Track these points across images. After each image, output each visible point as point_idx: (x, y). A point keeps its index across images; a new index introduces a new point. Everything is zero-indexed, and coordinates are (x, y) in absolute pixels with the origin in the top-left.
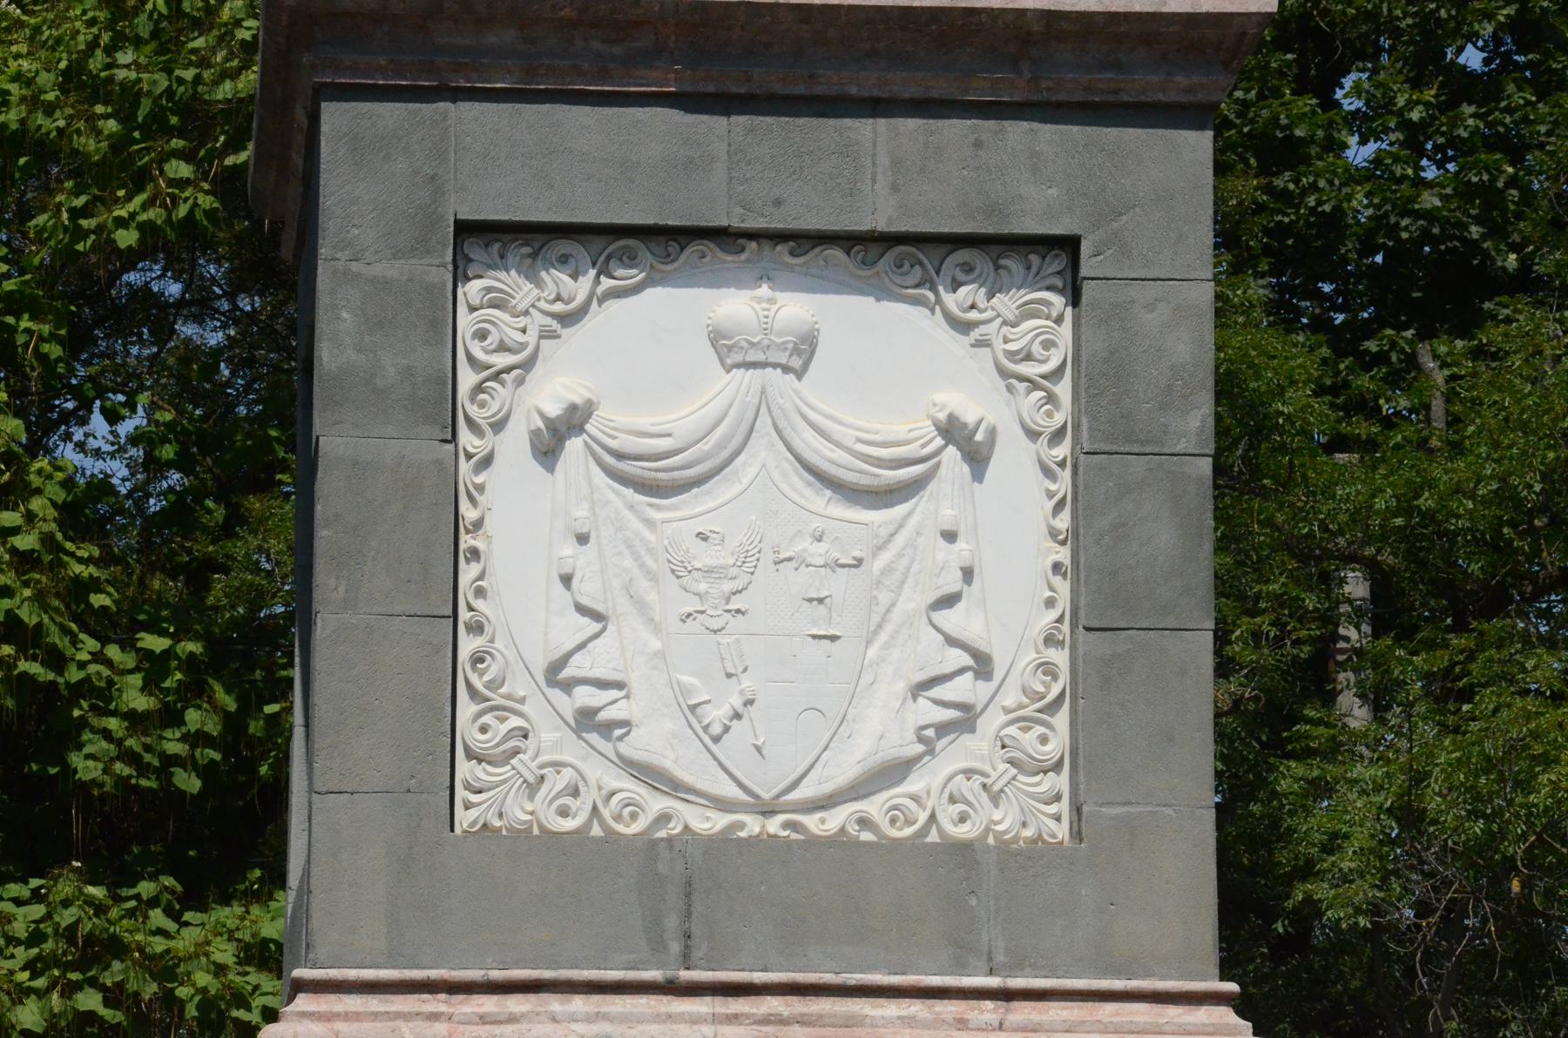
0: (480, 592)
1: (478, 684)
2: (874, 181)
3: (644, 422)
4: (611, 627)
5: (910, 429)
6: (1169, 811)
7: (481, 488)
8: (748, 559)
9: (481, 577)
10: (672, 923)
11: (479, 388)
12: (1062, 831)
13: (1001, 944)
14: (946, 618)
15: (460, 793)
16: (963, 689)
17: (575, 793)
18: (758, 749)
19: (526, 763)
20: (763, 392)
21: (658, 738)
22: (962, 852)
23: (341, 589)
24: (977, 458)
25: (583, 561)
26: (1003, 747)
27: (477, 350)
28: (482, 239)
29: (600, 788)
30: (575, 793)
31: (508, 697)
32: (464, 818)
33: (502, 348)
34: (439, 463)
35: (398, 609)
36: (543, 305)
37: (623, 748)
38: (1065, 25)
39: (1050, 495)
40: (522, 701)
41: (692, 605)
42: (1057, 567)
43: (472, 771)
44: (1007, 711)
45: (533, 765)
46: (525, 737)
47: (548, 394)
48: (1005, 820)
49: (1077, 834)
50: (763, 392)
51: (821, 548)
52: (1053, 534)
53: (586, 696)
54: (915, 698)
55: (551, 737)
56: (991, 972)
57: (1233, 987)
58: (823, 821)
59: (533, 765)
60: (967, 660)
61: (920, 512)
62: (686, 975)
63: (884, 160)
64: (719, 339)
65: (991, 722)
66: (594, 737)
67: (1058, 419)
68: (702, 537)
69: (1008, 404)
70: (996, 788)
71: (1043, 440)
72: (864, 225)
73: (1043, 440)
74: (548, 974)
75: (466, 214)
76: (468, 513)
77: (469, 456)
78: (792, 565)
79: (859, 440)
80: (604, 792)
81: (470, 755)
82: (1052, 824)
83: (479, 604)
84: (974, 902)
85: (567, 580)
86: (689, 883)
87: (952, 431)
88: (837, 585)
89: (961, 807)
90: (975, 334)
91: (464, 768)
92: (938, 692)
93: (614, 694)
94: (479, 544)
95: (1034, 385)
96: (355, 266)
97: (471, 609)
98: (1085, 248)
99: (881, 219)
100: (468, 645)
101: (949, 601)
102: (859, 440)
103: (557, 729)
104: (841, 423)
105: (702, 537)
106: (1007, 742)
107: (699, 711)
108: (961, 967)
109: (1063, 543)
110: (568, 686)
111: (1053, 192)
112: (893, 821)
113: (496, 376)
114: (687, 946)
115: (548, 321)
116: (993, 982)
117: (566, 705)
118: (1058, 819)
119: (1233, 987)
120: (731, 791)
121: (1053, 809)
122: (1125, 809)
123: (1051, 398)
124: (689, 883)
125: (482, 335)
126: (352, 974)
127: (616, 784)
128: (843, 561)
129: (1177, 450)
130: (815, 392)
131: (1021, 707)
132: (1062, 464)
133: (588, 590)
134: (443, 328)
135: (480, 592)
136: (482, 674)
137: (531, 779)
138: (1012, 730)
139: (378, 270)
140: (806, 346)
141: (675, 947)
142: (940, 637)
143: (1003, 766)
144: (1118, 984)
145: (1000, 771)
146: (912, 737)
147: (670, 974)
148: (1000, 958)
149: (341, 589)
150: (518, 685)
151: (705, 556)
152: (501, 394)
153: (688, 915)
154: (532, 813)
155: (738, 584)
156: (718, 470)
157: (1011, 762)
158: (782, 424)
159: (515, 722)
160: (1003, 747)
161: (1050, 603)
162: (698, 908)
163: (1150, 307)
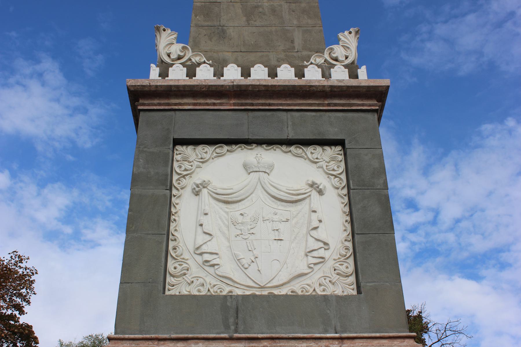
0: (176, 230)
1: (174, 255)
2: (287, 128)
3: (225, 186)
4: (214, 239)
5: (301, 185)
6: (388, 284)
7: (177, 204)
8: (255, 220)
9: (176, 226)
10: (231, 320)
11: (178, 180)
12: (355, 293)
13: (339, 324)
14: (314, 233)
15: (167, 286)
16: (322, 253)
17: (203, 285)
18: (259, 271)
19: (188, 278)
20: (259, 179)
21: (228, 268)
22: (325, 298)
23: (133, 227)
24: (321, 192)
25: (204, 220)
26: (335, 270)
27: (178, 170)
28: (178, 142)
29: (211, 284)
30: (203, 285)
31: (183, 259)
32: (167, 293)
33: (186, 170)
34: (165, 195)
35: (150, 232)
36: (197, 160)
37: (217, 272)
38: (335, 89)
39: (343, 203)
40: (187, 260)
41: (239, 232)
42: (346, 221)
43: (171, 280)
44: (334, 260)
45: (190, 278)
46: (188, 270)
47: (199, 177)
48: (339, 292)
49: (359, 292)
50: (259, 179)
51: (277, 217)
52: (345, 213)
53: (207, 257)
54: (307, 256)
55: (195, 270)
56: (336, 333)
57: (414, 334)
58: (280, 292)
59: (190, 278)
60: (322, 245)
61: (304, 207)
62: (236, 335)
63: (290, 123)
64: (246, 166)
65: (330, 263)
66: (207, 268)
67: (343, 185)
68: (242, 214)
69: (329, 182)
70: (333, 281)
71: (340, 189)
72: (284, 137)
73: (340, 189)
74: (190, 336)
75: (176, 137)
76: (173, 210)
77: (175, 196)
78: (268, 221)
79: (287, 189)
80: (212, 285)
81: (171, 275)
82: (352, 291)
83: (175, 233)
84: (329, 312)
85: (201, 225)
86: (237, 308)
87: (313, 185)
88: (281, 226)
89: (323, 287)
90: (318, 164)
91: (169, 279)
92: (315, 254)
93: (215, 256)
94: (177, 218)
95: (336, 176)
96: (145, 149)
97: (173, 235)
98: (346, 142)
99: (292, 135)
100: (171, 244)
101: (316, 228)
102: (287, 189)
103: (198, 268)
104: (281, 186)
105: (242, 214)
106: (336, 268)
107: (240, 261)
108: (326, 332)
109: (348, 215)
110: (201, 254)
111: (336, 129)
112: (302, 292)
113: (184, 177)
114: (236, 327)
115: (199, 163)
116: (337, 335)
117: (199, 259)
118: (353, 290)
119: (414, 334)
120: (252, 284)
121: (352, 287)
122: (374, 284)
123: (341, 179)
124: (237, 308)
125: (180, 167)
126: (127, 336)
127: (215, 283)
128: (283, 220)
129: (378, 188)
130: (274, 178)
131: (339, 258)
132: (345, 195)
133: (206, 229)
134: (168, 161)
135: (176, 230)
136: (175, 252)
137: (189, 282)
138: (337, 265)
139: (152, 150)
140: (271, 167)
141: (233, 328)
142: (314, 239)
143: (335, 275)
144: (378, 335)
145: (335, 277)
146: (306, 267)
147: (231, 334)
148: (338, 329)
149: (133, 227)
150: (186, 256)
151: (240, 219)
152: (184, 182)
153: (237, 317)
154: (189, 292)
155: (252, 227)
156: (246, 198)
157: (338, 274)
158: (264, 186)
159: (185, 265)
160: (335, 270)
161: (345, 230)
162: (240, 315)
163: (366, 155)
